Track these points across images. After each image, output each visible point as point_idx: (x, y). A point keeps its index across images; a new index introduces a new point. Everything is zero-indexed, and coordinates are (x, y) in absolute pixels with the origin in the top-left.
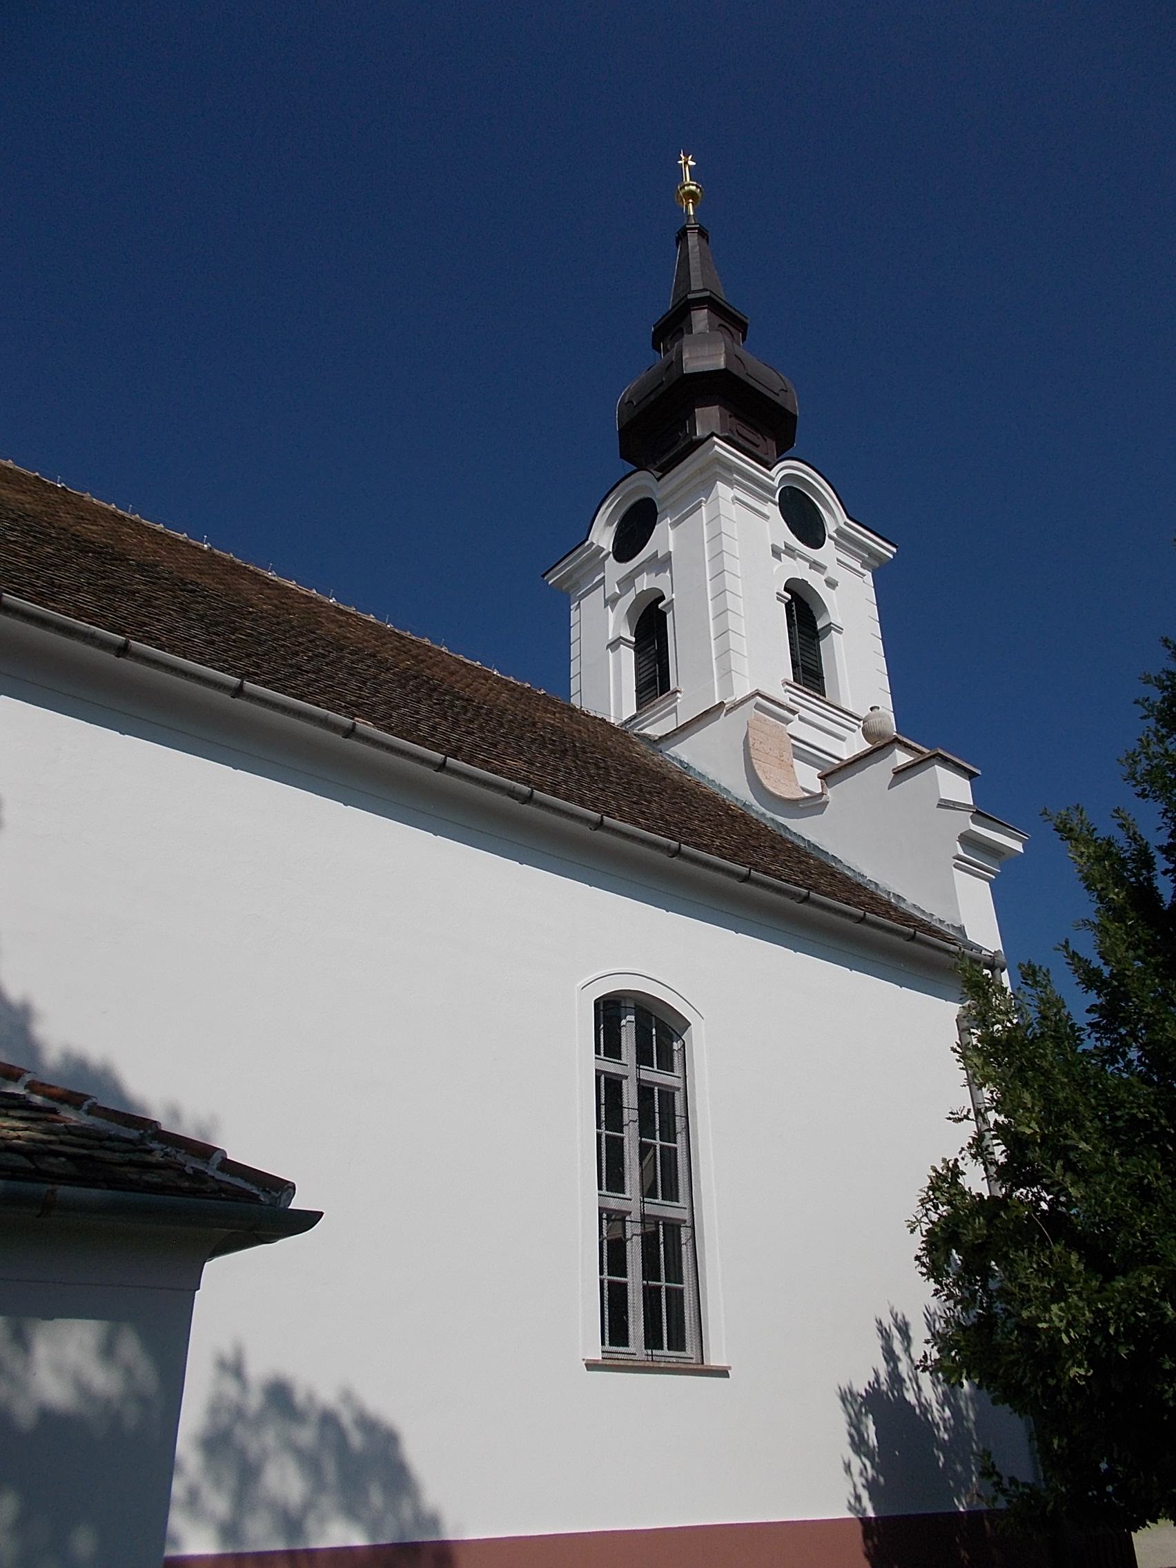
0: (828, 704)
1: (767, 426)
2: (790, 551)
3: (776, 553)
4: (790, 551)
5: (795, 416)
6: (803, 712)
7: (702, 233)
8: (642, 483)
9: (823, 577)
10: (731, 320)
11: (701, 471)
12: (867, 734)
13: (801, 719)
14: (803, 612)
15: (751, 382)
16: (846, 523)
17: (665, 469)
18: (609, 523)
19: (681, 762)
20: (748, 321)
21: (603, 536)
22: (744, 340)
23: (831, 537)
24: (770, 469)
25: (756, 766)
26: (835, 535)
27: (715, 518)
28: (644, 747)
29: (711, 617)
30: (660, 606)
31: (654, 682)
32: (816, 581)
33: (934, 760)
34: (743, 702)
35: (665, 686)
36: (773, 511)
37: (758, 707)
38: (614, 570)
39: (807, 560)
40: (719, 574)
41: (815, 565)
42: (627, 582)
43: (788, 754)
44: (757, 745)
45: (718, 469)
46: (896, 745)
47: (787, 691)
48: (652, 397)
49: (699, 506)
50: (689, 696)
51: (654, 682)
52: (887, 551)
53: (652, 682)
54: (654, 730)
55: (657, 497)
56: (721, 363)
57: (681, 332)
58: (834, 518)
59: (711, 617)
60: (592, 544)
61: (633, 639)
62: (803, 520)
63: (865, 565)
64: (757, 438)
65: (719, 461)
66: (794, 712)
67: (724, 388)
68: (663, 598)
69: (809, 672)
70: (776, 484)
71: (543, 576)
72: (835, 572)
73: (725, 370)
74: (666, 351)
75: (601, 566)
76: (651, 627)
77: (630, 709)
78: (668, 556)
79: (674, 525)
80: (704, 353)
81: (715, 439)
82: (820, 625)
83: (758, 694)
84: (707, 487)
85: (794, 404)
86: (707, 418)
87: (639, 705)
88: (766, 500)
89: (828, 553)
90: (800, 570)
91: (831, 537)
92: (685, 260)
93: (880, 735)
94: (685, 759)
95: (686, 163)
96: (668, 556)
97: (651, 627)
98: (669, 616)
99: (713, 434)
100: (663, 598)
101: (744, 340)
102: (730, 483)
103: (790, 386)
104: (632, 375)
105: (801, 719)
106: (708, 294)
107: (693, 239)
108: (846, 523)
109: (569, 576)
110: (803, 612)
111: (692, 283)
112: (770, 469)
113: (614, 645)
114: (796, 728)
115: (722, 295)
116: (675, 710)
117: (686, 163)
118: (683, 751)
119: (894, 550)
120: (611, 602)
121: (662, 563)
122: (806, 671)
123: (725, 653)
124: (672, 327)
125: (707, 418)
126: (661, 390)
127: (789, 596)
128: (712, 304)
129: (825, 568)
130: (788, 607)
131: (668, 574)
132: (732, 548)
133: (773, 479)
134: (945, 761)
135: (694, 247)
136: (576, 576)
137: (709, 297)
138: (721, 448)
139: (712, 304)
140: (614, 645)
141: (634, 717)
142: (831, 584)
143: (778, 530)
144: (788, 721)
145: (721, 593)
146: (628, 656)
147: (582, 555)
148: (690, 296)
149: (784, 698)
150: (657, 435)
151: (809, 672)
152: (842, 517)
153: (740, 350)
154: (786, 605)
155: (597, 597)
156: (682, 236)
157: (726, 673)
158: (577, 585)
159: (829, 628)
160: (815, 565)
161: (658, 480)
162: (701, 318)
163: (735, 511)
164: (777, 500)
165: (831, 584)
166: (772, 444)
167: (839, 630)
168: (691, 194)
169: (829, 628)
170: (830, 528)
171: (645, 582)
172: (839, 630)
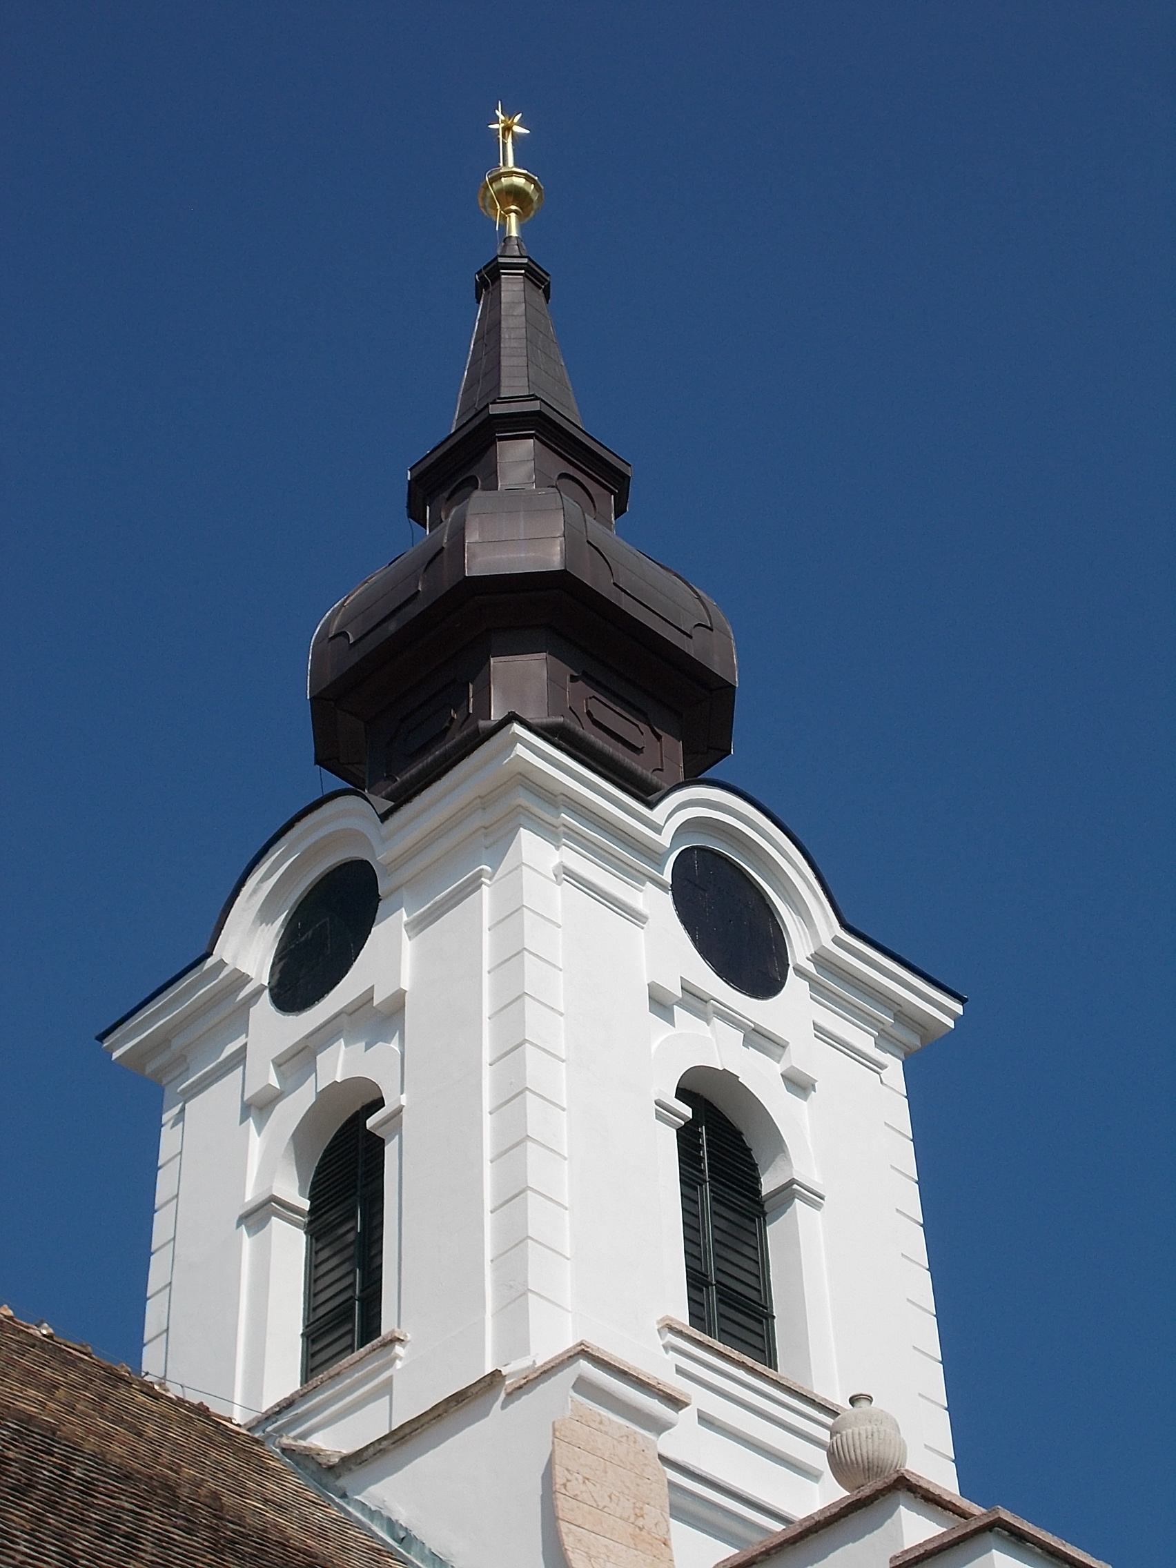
0: (776, 1384)
1: (656, 702)
2: (694, 999)
3: (660, 1004)
4: (694, 999)
5: (726, 690)
6: (701, 1399)
7: (535, 276)
8: (349, 825)
9: (779, 1068)
10: (589, 467)
11: (484, 802)
12: (841, 1465)
13: (705, 1420)
14: (722, 1154)
15: (626, 604)
16: (836, 940)
17: (402, 798)
18: (265, 915)
19: (391, 1525)
20: (629, 472)
21: (249, 947)
22: (620, 511)
23: (800, 972)
24: (651, 806)
25: (568, 1542)
26: (811, 968)
27: (511, 915)
28: (294, 1481)
29: (488, 1153)
30: (370, 1123)
31: (345, 1315)
32: (760, 1077)
33: (989, 1537)
34: (548, 1372)
35: (370, 1328)
36: (658, 905)
37: (583, 1386)
38: (271, 1030)
39: (737, 1024)
40: (512, 1049)
41: (759, 1038)
42: (299, 1060)
43: (657, 1510)
44: (575, 1487)
45: (523, 799)
46: (902, 1495)
47: (669, 1347)
48: (392, 627)
49: (474, 885)
50: (423, 1352)
51: (345, 1315)
52: (942, 1010)
53: (342, 1315)
54: (333, 1441)
55: (379, 858)
56: (552, 558)
57: (472, 483)
58: (809, 926)
59: (488, 1153)
60: (222, 964)
61: (305, 1205)
62: (732, 928)
63: (885, 1040)
64: (639, 734)
65: (526, 780)
66: (676, 1403)
67: (557, 611)
68: (379, 1103)
69: (732, 1300)
70: (665, 839)
71: (102, 1037)
72: (807, 1055)
73: (565, 571)
74: (436, 521)
75: (239, 1019)
76: (347, 1174)
77: (283, 1374)
78: (397, 1003)
79: (418, 926)
80: (517, 531)
81: (517, 728)
82: (768, 1184)
83: (583, 1352)
84: (496, 840)
85: (726, 656)
86: (521, 679)
87: (310, 1369)
88: (639, 878)
89: (792, 1008)
90: (719, 1048)
91: (800, 972)
92: (492, 332)
93: (870, 1468)
94: (402, 1515)
95: (507, 129)
96: (397, 1003)
97: (347, 1174)
98: (390, 1151)
99: (511, 718)
100: (379, 1103)
101: (620, 511)
102: (552, 834)
103: (720, 618)
104: (353, 573)
105: (705, 1420)
106: (535, 406)
107: (512, 288)
108: (836, 940)
109: (162, 1041)
110: (722, 1154)
111: (504, 382)
112: (651, 806)
113: (257, 1216)
114: (685, 1440)
115: (571, 411)
116: (386, 1388)
117: (507, 129)
118: (395, 1495)
119: (958, 1008)
120: (258, 1108)
121: (382, 1019)
122: (729, 1298)
123: (515, 1244)
124: (453, 472)
125: (521, 679)
126: (414, 610)
127: (688, 1111)
128: (542, 426)
129: (783, 1045)
130: (686, 1137)
131: (395, 1045)
132: (549, 981)
133: (658, 829)
134: (1018, 1540)
135: (513, 304)
136: (177, 1044)
137: (538, 413)
138: (530, 752)
139: (542, 426)
140: (257, 1216)
141: (288, 1404)
142: (798, 1085)
143: (665, 946)
144: (660, 1427)
145: (514, 1097)
146: (289, 1245)
147: (195, 991)
148: (495, 410)
149: (658, 1363)
150: (397, 710)
151: (732, 1300)
152: (827, 926)
153: (607, 535)
154: (680, 1131)
155: (224, 1096)
156: (490, 277)
157: (516, 1296)
158: (181, 1063)
159: (787, 1192)
160: (759, 1038)
161: (384, 817)
162: (518, 458)
163: (564, 897)
164: (667, 877)
165: (798, 1085)
166: (673, 747)
167: (815, 1199)
168: (516, 194)
169: (787, 1192)
170: (799, 950)
171: (340, 1063)
172: (815, 1199)
